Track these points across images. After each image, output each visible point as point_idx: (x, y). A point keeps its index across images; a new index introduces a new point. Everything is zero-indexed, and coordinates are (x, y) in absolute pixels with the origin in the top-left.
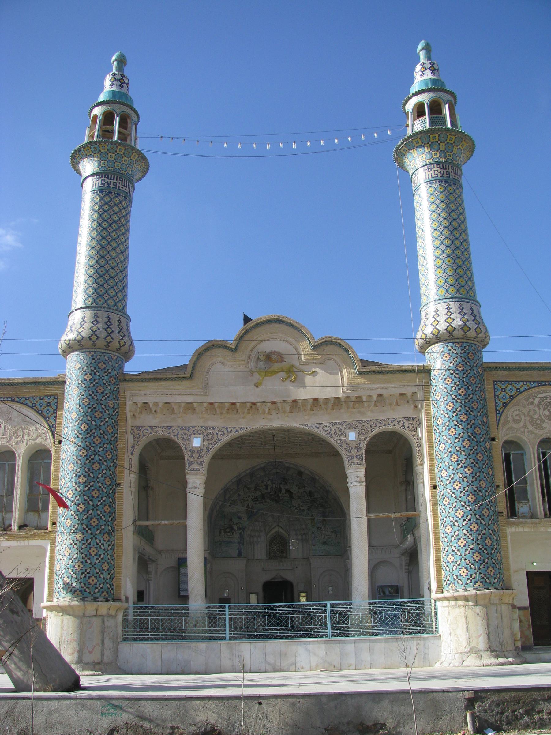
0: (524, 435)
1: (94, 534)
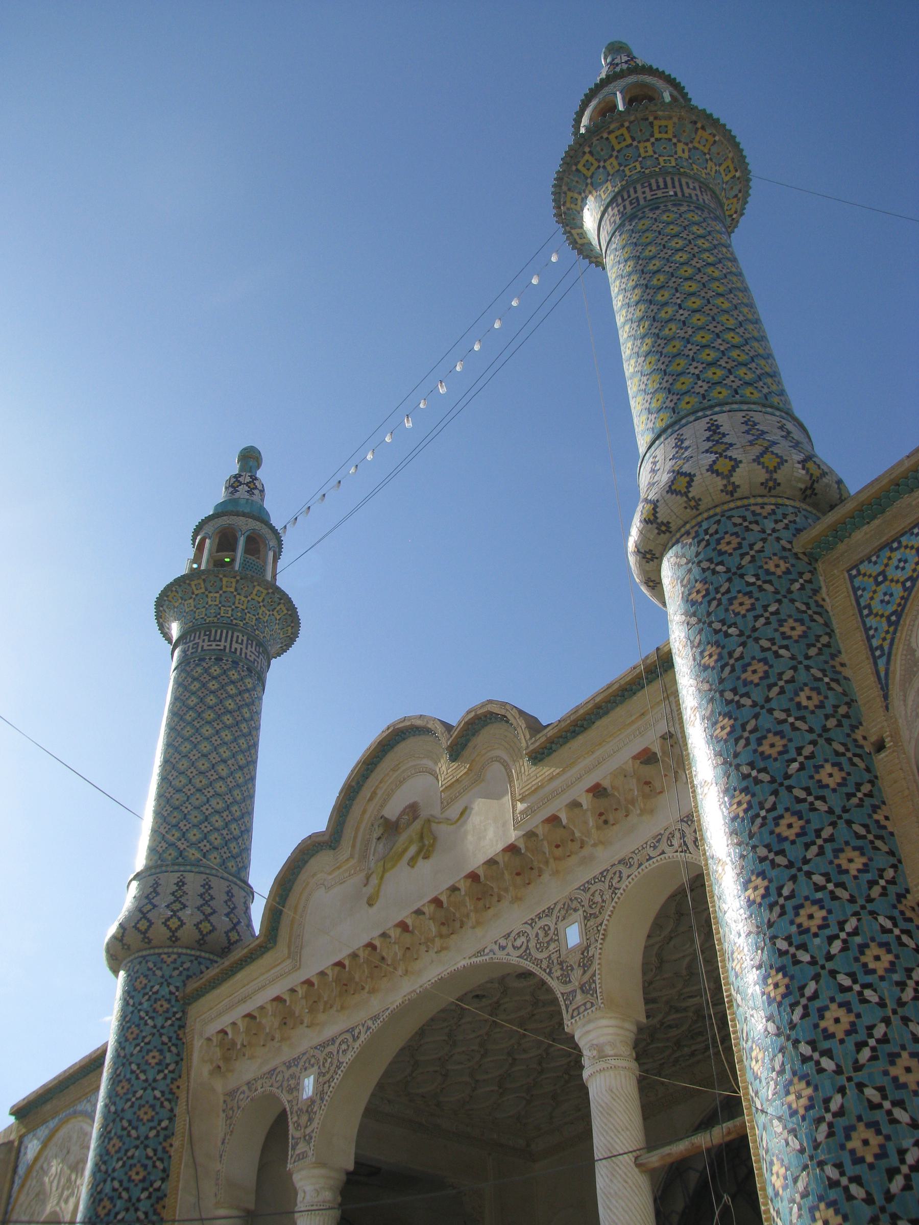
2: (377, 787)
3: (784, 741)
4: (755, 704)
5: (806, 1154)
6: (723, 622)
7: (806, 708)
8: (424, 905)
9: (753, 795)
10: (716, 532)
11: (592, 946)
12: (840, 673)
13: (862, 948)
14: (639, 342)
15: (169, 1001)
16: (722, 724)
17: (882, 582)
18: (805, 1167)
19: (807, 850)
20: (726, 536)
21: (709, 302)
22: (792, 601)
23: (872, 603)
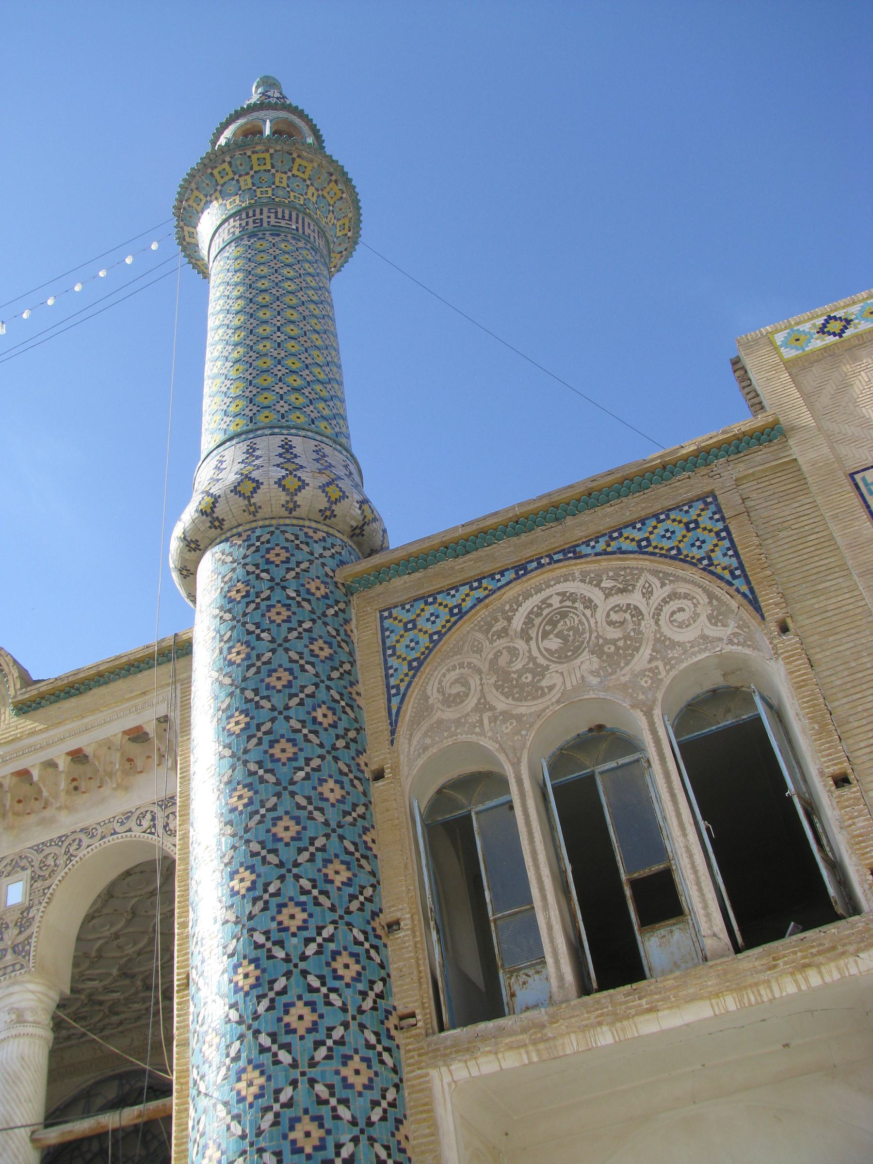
0: (483, 734)
3: (295, 750)
4: (274, 709)
5: (247, 1140)
6: (258, 626)
7: (321, 724)
9: (256, 792)
10: (268, 542)
11: (34, 908)
12: (355, 701)
13: (335, 954)
14: (231, 348)
16: (237, 719)
17: (411, 629)
18: (244, 1153)
19: (299, 854)
20: (277, 548)
21: (305, 334)
22: (325, 624)
23: (398, 645)
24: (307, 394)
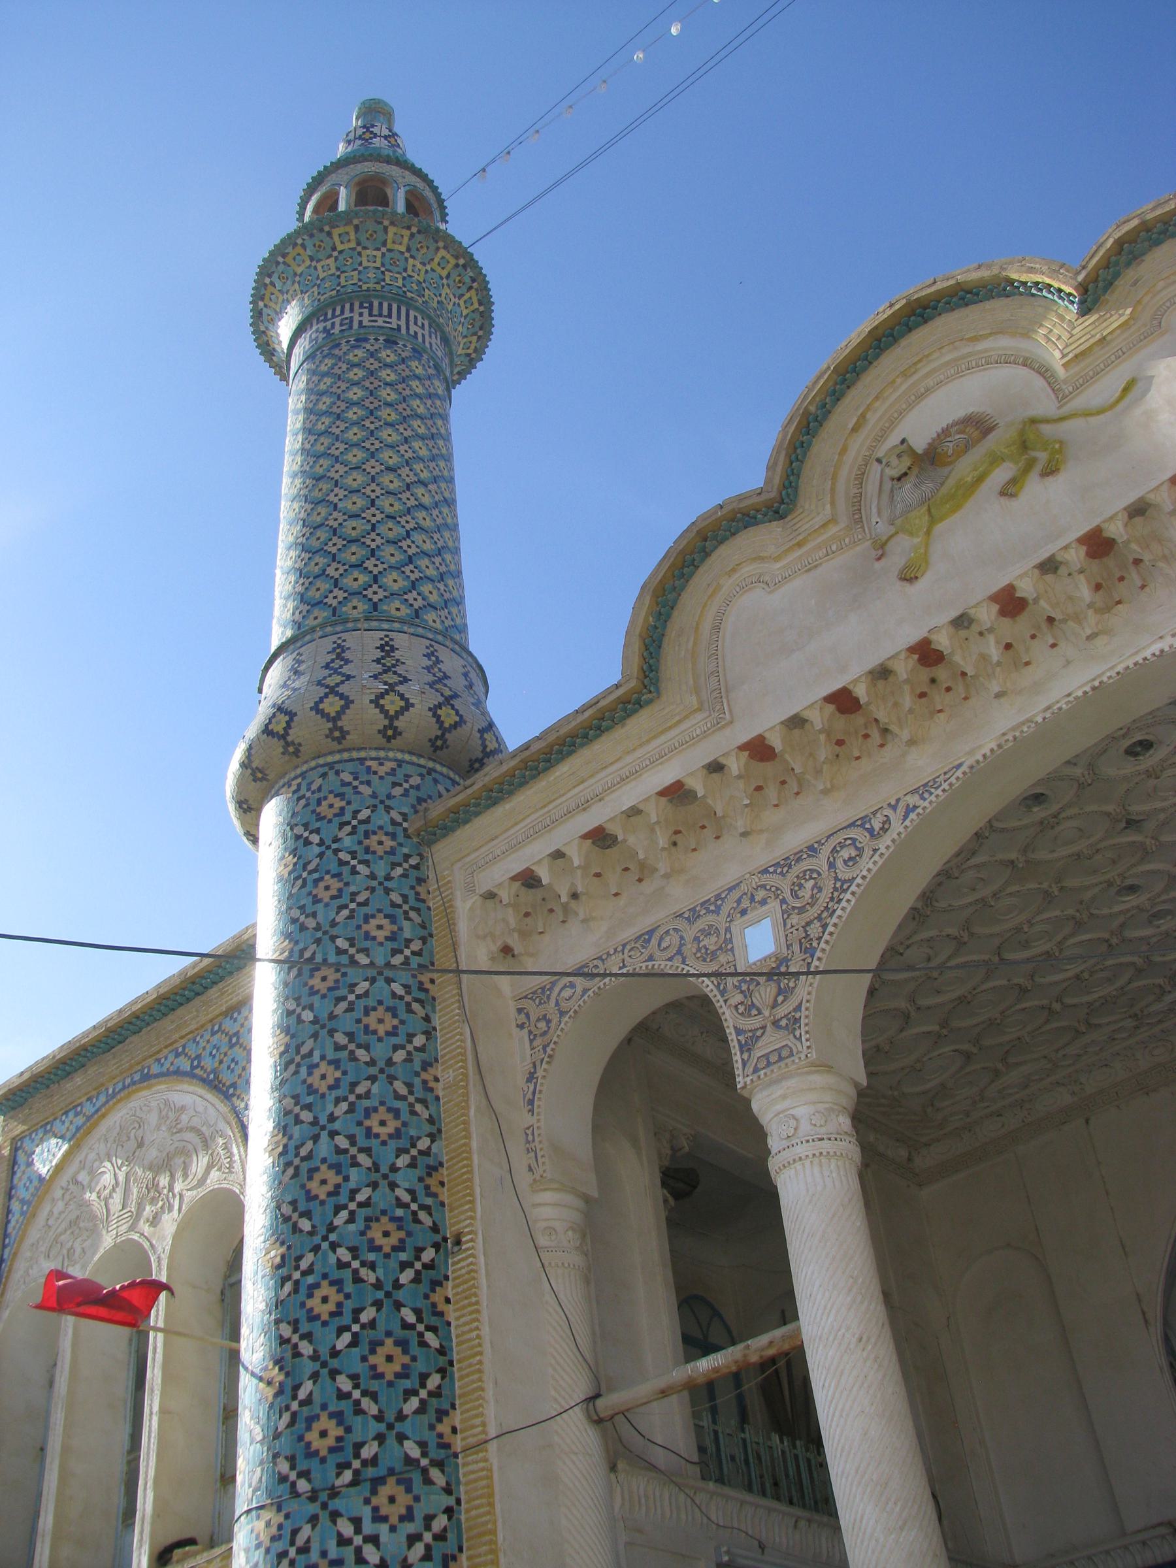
1: (323, 1496)
2: (868, 408)
8: (1066, 548)
15: (393, 836)
24: (402, 430)
